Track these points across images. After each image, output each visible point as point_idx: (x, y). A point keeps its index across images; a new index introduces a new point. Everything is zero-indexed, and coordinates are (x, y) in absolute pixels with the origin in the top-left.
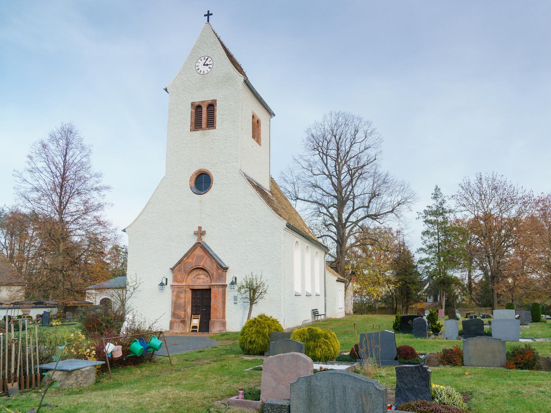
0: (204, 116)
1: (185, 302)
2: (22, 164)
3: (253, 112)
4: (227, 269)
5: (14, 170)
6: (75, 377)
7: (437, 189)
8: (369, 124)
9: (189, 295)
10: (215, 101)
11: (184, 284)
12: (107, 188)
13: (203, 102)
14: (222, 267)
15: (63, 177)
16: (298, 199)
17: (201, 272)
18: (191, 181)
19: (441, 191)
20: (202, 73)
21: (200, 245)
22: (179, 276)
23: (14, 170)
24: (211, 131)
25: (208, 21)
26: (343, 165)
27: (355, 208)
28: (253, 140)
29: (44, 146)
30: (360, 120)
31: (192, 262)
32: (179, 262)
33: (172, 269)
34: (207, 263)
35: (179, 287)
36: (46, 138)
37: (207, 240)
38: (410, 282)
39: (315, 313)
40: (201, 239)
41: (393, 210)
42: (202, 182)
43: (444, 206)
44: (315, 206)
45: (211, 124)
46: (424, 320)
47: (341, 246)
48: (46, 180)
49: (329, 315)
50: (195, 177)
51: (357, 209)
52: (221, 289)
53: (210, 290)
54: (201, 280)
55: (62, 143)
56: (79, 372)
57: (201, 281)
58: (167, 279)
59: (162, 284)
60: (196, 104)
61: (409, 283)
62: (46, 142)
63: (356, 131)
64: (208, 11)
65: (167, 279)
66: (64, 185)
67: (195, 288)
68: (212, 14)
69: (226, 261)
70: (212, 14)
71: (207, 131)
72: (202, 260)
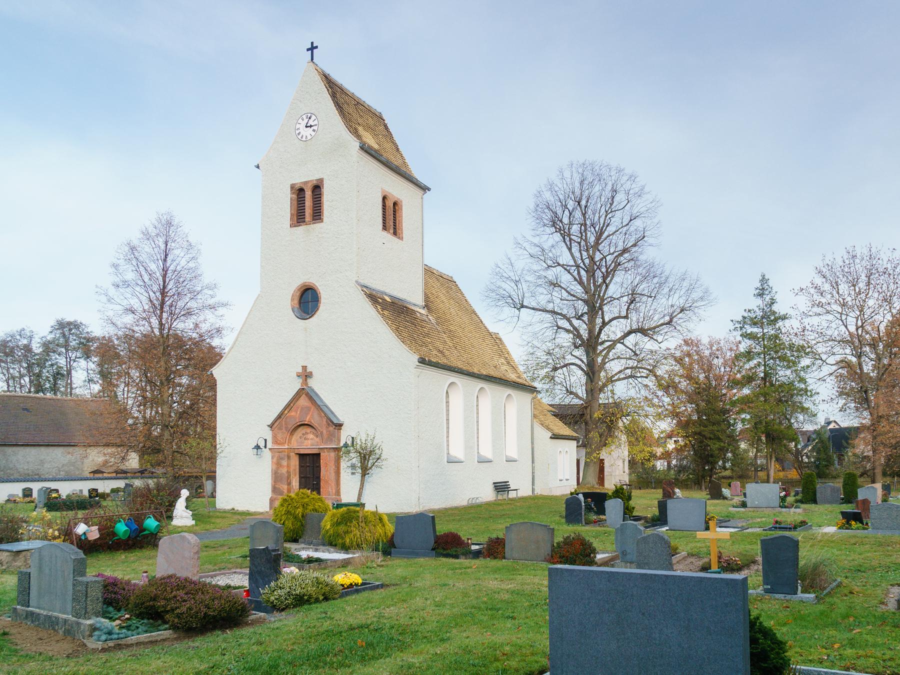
0: (307, 203)
1: (288, 472)
2: (107, 279)
3: (383, 191)
4: (340, 425)
5: (97, 287)
6: (23, 559)
7: (764, 280)
8: (632, 178)
9: (295, 462)
10: (321, 180)
11: (286, 447)
12: (224, 305)
13: (306, 183)
14: (332, 422)
15: (163, 292)
16: (522, 306)
17: (309, 430)
18: (292, 300)
19: (770, 283)
20: (304, 139)
21: (305, 393)
22: (279, 436)
23: (97, 287)
24: (317, 226)
25: (312, 59)
26: (592, 247)
27: (607, 319)
28: (385, 233)
29: (133, 249)
30: (620, 171)
31: (295, 416)
32: (279, 417)
33: (271, 426)
34: (313, 417)
35: (280, 451)
36: (135, 237)
37: (314, 384)
38: (712, 436)
39: (501, 487)
40: (307, 384)
41: (671, 321)
42: (307, 300)
43: (775, 308)
44: (548, 316)
45: (317, 215)
46: (579, 500)
47: (592, 381)
48: (140, 300)
49: (538, 491)
50: (298, 294)
51: (611, 321)
52: (333, 454)
53: (318, 455)
54: (309, 442)
55: (161, 242)
56: (29, 554)
57: (308, 443)
58: (266, 440)
59: (258, 447)
60: (297, 187)
61: (710, 439)
62: (135, 242)
63: (615, 191)
64: (312, 43)
65: (266, 440)
66: (163, 301)
67: (302, 452)
68: (316, 47)
69: (340, 412)
70: (316, 47)
71: (312, 226)
72: (308, 414)
